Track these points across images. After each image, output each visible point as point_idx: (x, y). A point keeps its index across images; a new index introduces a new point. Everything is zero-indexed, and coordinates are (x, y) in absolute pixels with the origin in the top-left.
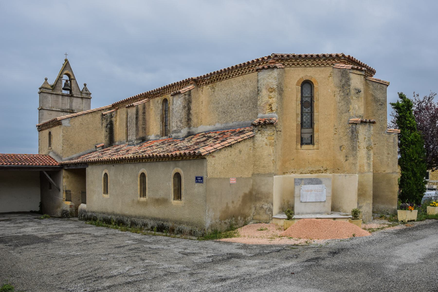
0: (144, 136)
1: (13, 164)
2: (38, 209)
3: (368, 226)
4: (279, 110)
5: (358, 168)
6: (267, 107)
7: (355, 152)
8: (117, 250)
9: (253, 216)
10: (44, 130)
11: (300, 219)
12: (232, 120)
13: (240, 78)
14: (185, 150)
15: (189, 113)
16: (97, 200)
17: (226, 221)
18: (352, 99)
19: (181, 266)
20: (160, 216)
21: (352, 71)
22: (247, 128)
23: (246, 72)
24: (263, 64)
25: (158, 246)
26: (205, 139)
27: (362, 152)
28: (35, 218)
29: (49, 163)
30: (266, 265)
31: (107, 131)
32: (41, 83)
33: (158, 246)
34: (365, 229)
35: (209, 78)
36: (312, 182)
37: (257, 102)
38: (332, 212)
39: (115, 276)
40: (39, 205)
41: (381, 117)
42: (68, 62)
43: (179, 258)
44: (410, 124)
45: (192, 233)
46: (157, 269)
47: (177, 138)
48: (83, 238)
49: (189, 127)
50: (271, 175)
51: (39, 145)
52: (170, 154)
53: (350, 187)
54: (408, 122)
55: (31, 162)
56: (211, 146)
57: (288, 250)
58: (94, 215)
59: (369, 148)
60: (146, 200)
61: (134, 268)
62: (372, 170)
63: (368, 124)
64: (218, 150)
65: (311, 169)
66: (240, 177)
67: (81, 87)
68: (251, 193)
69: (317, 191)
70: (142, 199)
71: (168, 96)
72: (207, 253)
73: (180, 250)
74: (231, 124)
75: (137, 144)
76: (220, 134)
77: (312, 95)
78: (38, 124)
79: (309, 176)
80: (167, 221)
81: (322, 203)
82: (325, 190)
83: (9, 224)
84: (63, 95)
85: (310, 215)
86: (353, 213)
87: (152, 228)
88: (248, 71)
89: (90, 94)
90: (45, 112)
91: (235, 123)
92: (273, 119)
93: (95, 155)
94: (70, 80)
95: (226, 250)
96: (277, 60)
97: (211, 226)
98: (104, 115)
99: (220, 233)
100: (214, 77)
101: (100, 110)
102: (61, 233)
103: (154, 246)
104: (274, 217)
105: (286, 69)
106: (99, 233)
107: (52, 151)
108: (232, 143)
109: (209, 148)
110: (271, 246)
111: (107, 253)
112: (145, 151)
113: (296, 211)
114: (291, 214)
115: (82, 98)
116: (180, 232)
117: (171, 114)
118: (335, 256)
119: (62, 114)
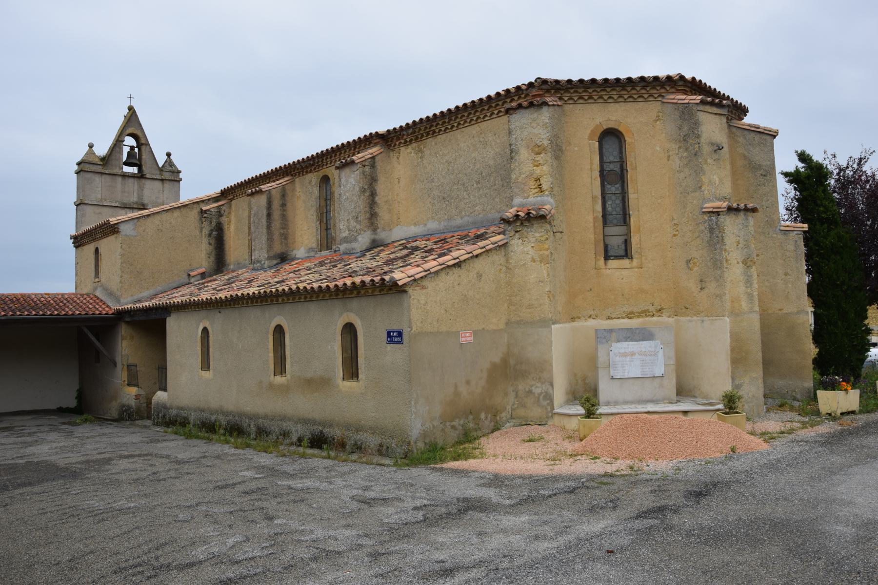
0: (283, 251)
1: (18, 313)
2: (72, 403)
3: (761, 426)
4: (556, 189)
5: (728, 305)
6: (532, 184)
7: (719, 272)
8: (218, 494)
9: (513, 410)
10: (85, 244)
11: (612, 414)
12: (460, 212)
13: (474, 129)
14: (363, 275)
15: (372, 203)
16: (189, 383)
17: (456, 423)
18: (706, 162)
19: (354, 532)
20: (316, 415)
21: (701, 108)
22: (492, 229)
23: (486, 116)
24: (519, 98)
25: (308, 483)
26: (405, 252)
27: (735, 271)
28: (64, 423)
29: (94, 309)
30: (546, 528)
31: (210, 244)
32: (80, 154)
33: (308, 483)
34: (752, 433)
35: (410, 131)
36: (631, 335)
37: (510, 175)
38: (679, 398)
39: (200, 562)
40: (75, 395)
41: (765, 199)
42: (134, 112)
43: (351, 514)
44: (825, 213)
45: (383, 451)
46: (298, 541)
47: (349, 253)
48: (151, 465)
49: (375, 230)
50: (546, 323)
51: (76, 275)
52: (332, 285)
53: (713, 345)
54: (822, 209)
55: (57, 310)
56: (418, 266)
57: (594, 488)
58: (183, 414)
59: (747, 262)
60: (286, 382)
61: (248, 540)
62: (757, 309)
63: (742, 213)
64: (430, 275)
65: (628, 310)
66: (480, 328)
67: (161, 160)
68: (505, 361)
69: (646, 355)
70: (279, 380)
71: (331, 171)
72: (413, 498)
73: (355, 492)
74: (458, 221)
75: (271, 267)
76: (436, 243)
77: (621, 158)
78: (74, 233)
79: (625, 323)
80: (331, 426)
81: (657, 380)
82: (661, 351)
83: (7, 436)
84: (125, 176)
85: (633, 406)
86: (726, 400)
87: (300, 440)
88: (488, 114)
89: (179, 172)
90: (89, 209)
91: (466, 219)
92: (546, 207)
93: (184, 292)
94: (139, 146)
95: (457, 489)
96: (548, 91)
97: (424, 435)
98: (205, 212)
99: (442, 449)
100: (420, 130)
101: (197, 202)
102: (107, 456)
103: (298, 484)
104: (556, 411)
105: (568, 108)
106: (187, 453)
107: (102, 286)
108: (462, 258)
109: (412, 271)
110: (554, 479)
111: (194, 502)
112: (283, 281)
113: (603, 396)
114: (593, 405)
115: (162, 180)
116: (358, 448)
117: (336, 205)
118: (702, 504)
119: (123, 211)
